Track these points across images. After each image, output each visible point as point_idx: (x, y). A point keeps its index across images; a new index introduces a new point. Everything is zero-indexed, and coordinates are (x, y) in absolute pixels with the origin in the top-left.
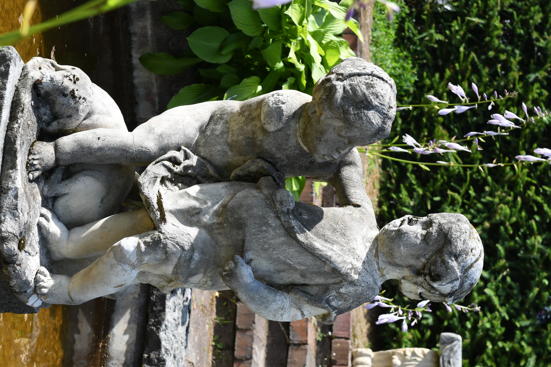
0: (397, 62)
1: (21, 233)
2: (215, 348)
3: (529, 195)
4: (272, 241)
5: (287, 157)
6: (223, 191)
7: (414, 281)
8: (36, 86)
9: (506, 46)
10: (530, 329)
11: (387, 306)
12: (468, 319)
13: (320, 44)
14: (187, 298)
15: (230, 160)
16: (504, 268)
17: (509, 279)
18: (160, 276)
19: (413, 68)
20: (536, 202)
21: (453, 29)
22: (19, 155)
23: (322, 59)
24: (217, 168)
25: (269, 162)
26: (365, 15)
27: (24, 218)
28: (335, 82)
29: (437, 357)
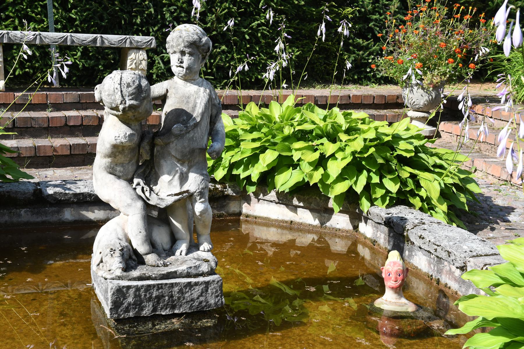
4: (200, 134)
28: (127, 105)
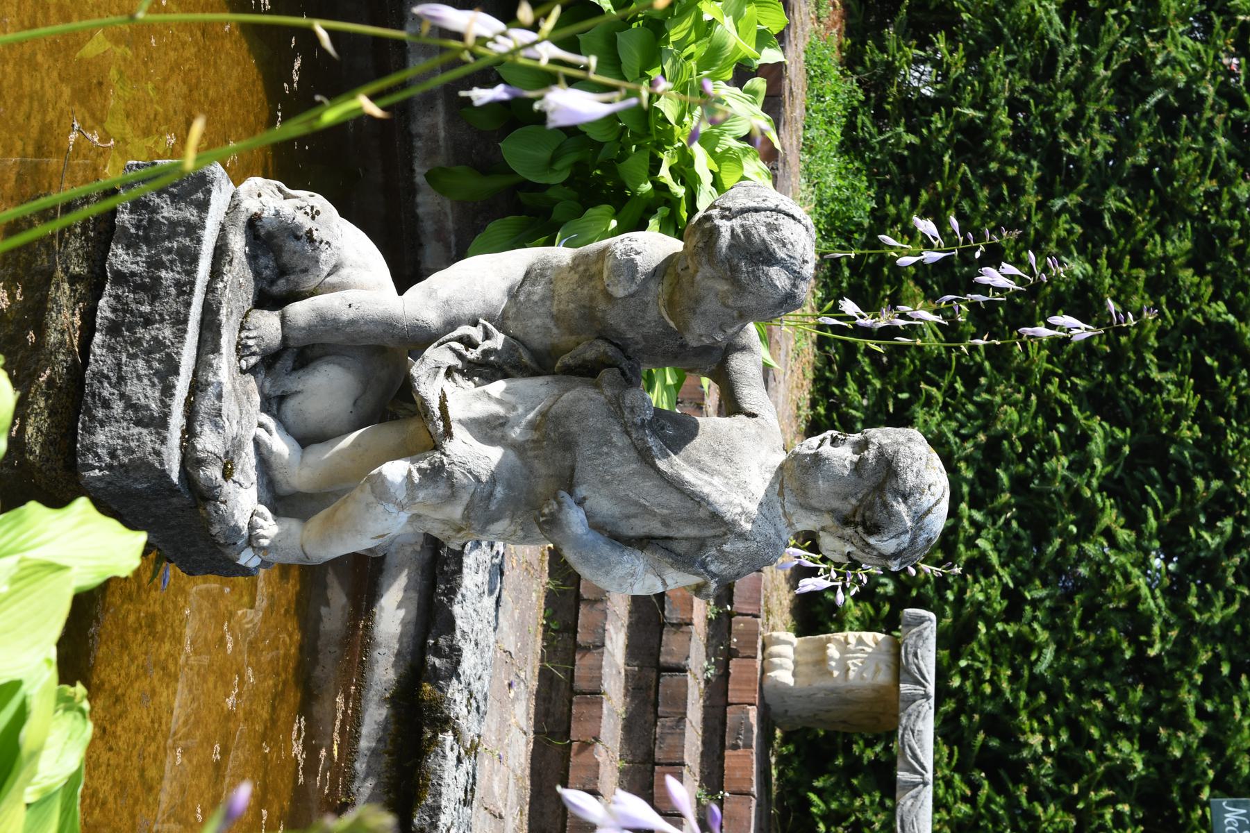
0: (843, 178)
1: (227, 452)
2: (546, 628)
3: (1049, 391)
4: (617, 470)
5: (645, 338)
6: (543, 390)
7: (840, 532)
8: (253, 223)
9: (1017, 154)
10: (1048, 603)
11: (813, 565)
12: (950, 587)
13: (712, 154)
14: (498, 553)
15: (556, 341)
16: (1008, 506)
17: (1014, 524)
18: (444, 522)
19: (868, 188)
20: (1060, 403)
21: (933, 126)
22: (224, 331)
23: (714, 178)
24: (534, 353)
25: (616, 345)
26: (792, 105)
27: (231, 429)
28: (718, 222)
29: (896, 646)
